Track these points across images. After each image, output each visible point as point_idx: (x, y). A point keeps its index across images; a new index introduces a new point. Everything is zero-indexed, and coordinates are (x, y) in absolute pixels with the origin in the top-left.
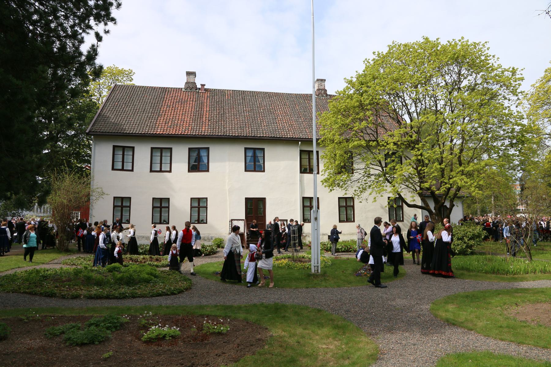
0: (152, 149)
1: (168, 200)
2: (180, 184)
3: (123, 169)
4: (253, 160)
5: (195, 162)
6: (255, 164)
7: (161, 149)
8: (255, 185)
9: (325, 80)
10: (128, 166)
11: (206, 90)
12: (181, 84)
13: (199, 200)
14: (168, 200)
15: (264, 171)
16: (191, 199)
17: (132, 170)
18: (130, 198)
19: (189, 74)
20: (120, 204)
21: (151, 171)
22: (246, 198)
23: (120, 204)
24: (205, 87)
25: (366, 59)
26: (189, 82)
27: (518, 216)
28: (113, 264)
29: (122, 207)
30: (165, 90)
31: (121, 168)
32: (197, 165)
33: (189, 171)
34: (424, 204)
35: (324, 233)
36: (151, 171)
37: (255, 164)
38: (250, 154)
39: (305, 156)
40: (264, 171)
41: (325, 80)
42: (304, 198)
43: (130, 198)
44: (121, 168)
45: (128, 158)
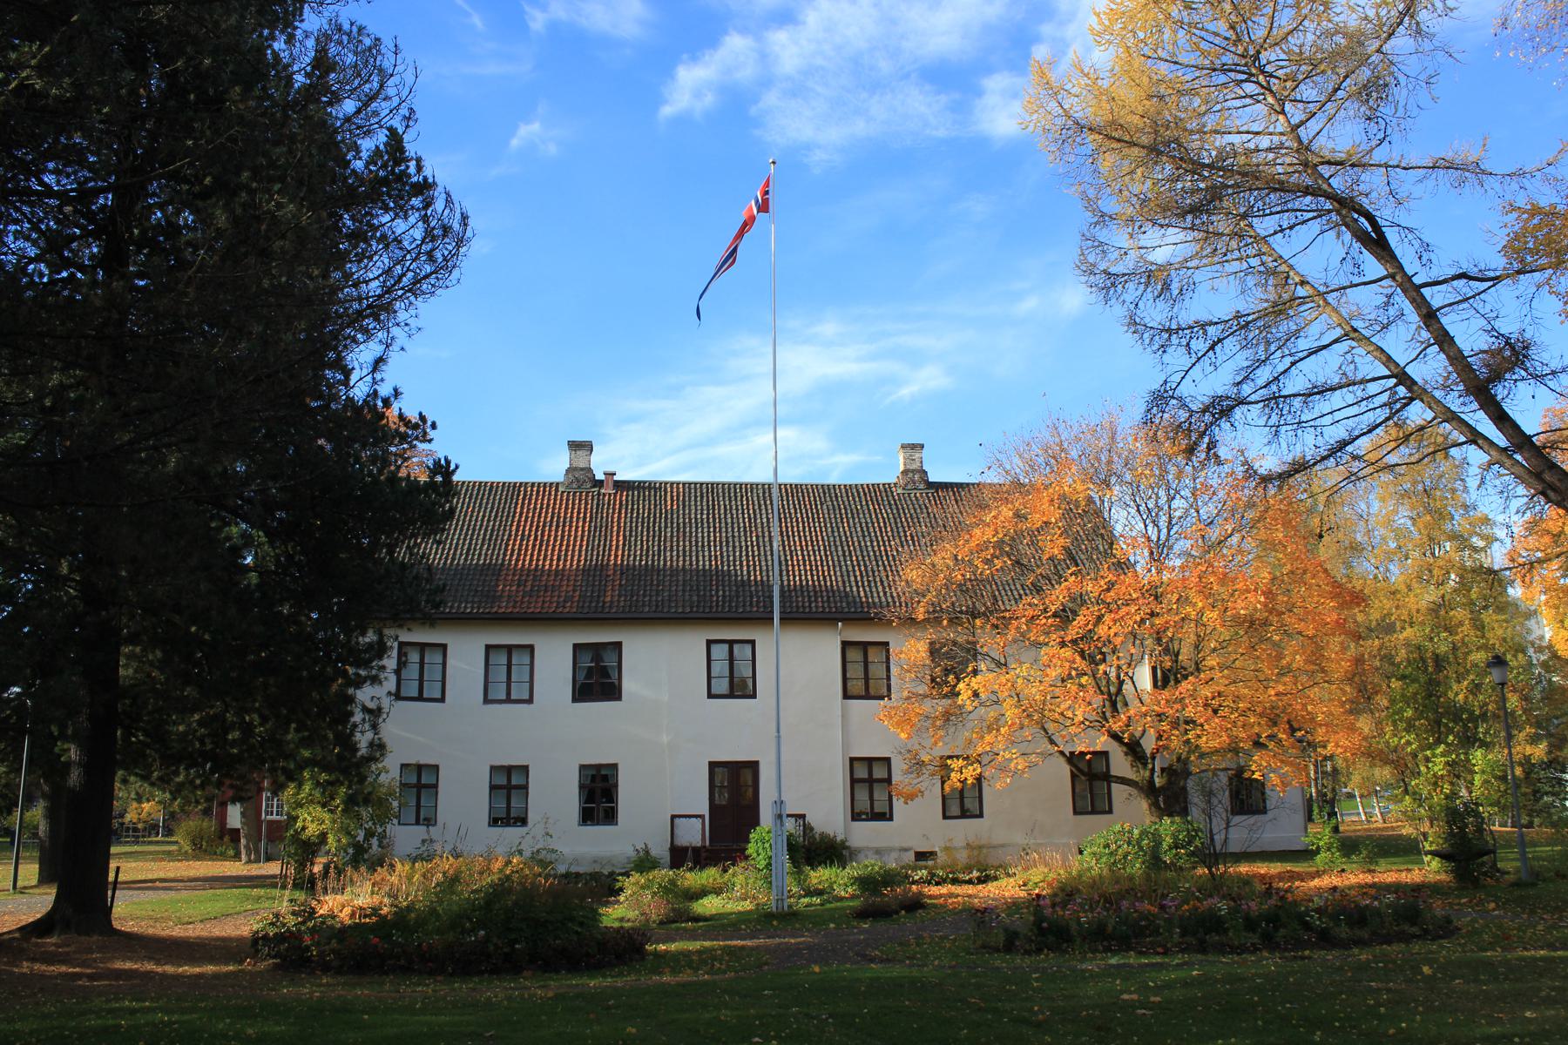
1: (525, 769)
2: (556, 734)
3: (509, 700)
7: (510, 649)
8: (736, 732)
9: (922, 446)
10: (432, 690)
11: (620, 485)
14: (525, 769)
15: (754, 696)
17: (442, 700)
18: (437, 767)
19: (575, 446)
21: (487, 701)
23: (504, 781)
25: (378, 39)
27: (25, 967)
30: (515, 490)
31: (416, 694)
32: (597, 681)
33: (575, 700)
35: (905, 845)
36: (487, 701)
38: (720, 652)
39: (855, 655)
40: (754, 696)
41: (922, 446)
42: (852, 760)
43: (437, 767)
44: (416, 694)
45: (432, 673)
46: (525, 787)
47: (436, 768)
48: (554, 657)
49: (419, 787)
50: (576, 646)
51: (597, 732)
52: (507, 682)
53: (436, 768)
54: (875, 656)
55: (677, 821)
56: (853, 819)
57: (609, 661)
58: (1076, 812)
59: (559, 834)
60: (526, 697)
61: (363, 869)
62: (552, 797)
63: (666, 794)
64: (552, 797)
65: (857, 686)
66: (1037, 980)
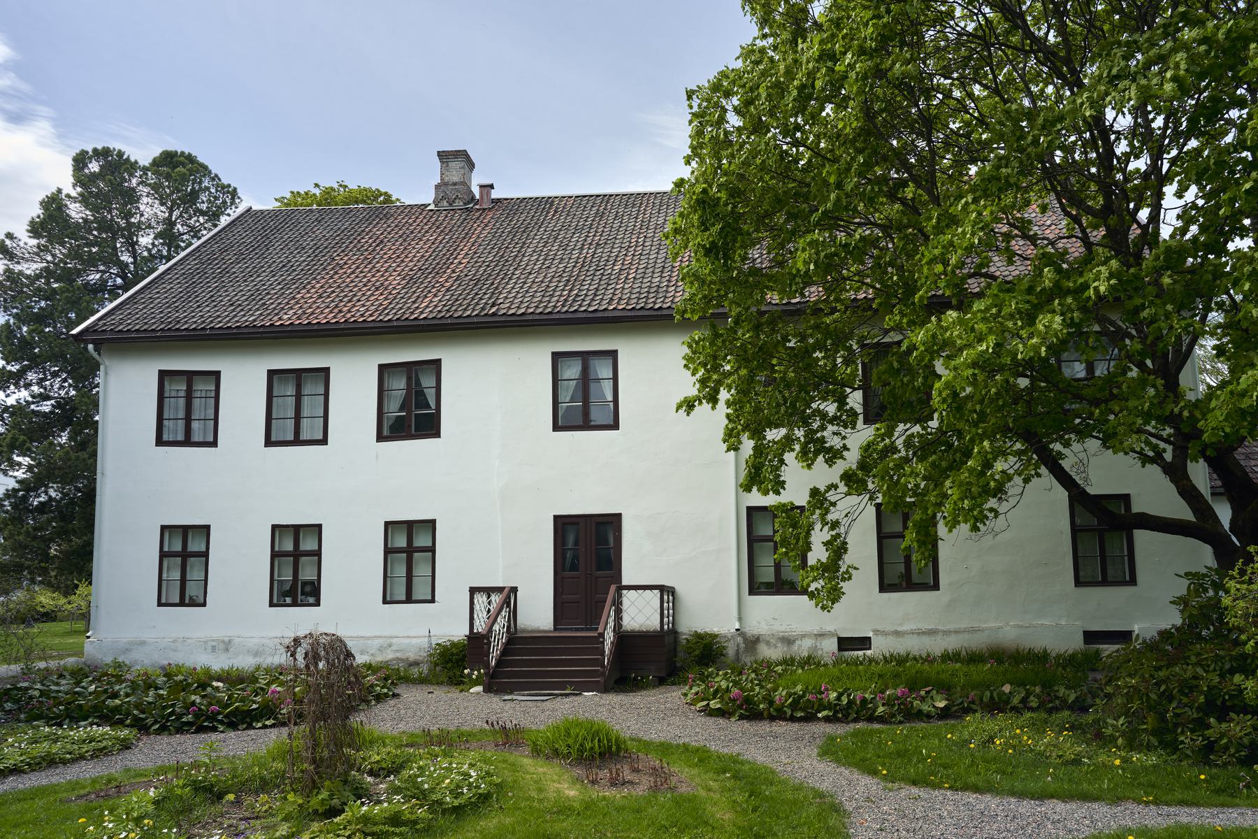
0: (556, 356)
2: (352, 480)
4: (580, 394)
5: (401, 410)
6: (583, 406)
8: (587, 476)
12: (416, 187)
13: (410, 527)
16: (387, 524)
19: (445, 157)
20: (178, 547)
22: (556, 518)
23: (178, 547)
24: (495, 194)
26: (446, 184)
28: (936, 400)
29: (185, 555)
31: (290, 437)
32: (411, 414)
34: (1195, 511)
37: (583, 406)
43: (208, 528)
44: (290, 437)
46: (318, 554)
47: (432, 524)
48: (354, 383)
49: (410, 551)
50: (272, 374)
51: (410, 477)
52: (295, 416)
53: (432, 524)
54: (201, 387)
55: (429, 598)
56: (751, 592)
57: (427, 382)
58: (1078, 583)
59: (358, 613)
60: (320, 437)
61: (964, 653)
62: (240, 565)
63: (501, 557)
64: (240, 565)
65: (175, 430)
66: (85, 826)
